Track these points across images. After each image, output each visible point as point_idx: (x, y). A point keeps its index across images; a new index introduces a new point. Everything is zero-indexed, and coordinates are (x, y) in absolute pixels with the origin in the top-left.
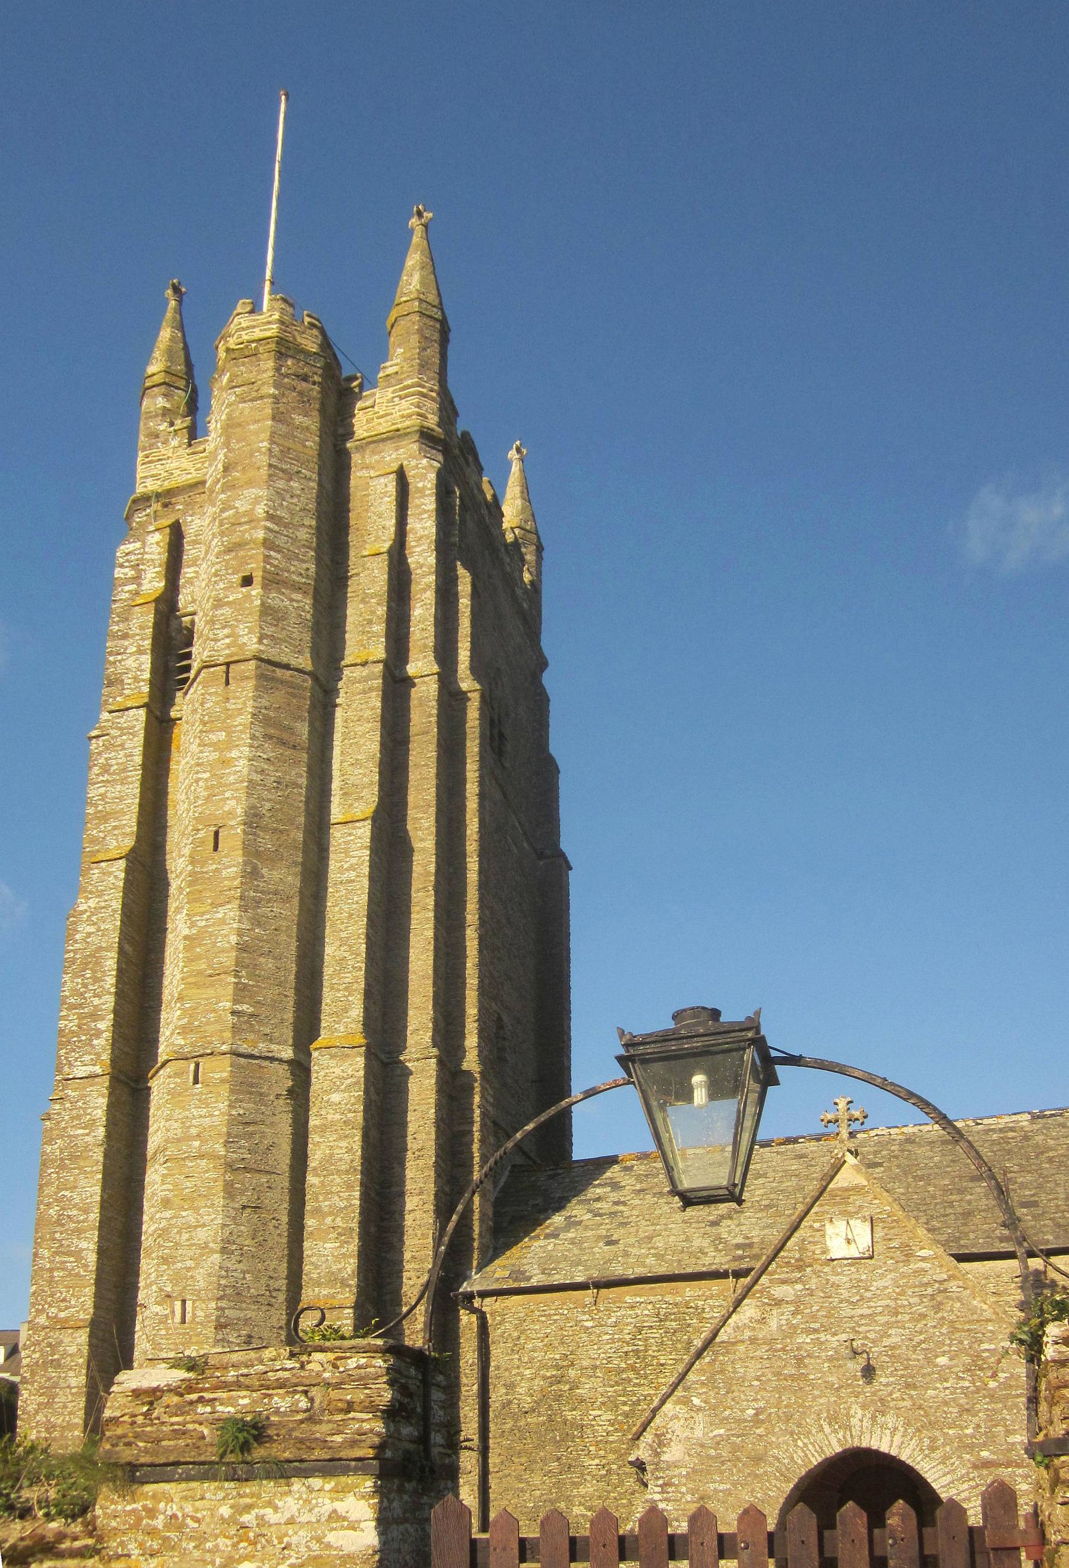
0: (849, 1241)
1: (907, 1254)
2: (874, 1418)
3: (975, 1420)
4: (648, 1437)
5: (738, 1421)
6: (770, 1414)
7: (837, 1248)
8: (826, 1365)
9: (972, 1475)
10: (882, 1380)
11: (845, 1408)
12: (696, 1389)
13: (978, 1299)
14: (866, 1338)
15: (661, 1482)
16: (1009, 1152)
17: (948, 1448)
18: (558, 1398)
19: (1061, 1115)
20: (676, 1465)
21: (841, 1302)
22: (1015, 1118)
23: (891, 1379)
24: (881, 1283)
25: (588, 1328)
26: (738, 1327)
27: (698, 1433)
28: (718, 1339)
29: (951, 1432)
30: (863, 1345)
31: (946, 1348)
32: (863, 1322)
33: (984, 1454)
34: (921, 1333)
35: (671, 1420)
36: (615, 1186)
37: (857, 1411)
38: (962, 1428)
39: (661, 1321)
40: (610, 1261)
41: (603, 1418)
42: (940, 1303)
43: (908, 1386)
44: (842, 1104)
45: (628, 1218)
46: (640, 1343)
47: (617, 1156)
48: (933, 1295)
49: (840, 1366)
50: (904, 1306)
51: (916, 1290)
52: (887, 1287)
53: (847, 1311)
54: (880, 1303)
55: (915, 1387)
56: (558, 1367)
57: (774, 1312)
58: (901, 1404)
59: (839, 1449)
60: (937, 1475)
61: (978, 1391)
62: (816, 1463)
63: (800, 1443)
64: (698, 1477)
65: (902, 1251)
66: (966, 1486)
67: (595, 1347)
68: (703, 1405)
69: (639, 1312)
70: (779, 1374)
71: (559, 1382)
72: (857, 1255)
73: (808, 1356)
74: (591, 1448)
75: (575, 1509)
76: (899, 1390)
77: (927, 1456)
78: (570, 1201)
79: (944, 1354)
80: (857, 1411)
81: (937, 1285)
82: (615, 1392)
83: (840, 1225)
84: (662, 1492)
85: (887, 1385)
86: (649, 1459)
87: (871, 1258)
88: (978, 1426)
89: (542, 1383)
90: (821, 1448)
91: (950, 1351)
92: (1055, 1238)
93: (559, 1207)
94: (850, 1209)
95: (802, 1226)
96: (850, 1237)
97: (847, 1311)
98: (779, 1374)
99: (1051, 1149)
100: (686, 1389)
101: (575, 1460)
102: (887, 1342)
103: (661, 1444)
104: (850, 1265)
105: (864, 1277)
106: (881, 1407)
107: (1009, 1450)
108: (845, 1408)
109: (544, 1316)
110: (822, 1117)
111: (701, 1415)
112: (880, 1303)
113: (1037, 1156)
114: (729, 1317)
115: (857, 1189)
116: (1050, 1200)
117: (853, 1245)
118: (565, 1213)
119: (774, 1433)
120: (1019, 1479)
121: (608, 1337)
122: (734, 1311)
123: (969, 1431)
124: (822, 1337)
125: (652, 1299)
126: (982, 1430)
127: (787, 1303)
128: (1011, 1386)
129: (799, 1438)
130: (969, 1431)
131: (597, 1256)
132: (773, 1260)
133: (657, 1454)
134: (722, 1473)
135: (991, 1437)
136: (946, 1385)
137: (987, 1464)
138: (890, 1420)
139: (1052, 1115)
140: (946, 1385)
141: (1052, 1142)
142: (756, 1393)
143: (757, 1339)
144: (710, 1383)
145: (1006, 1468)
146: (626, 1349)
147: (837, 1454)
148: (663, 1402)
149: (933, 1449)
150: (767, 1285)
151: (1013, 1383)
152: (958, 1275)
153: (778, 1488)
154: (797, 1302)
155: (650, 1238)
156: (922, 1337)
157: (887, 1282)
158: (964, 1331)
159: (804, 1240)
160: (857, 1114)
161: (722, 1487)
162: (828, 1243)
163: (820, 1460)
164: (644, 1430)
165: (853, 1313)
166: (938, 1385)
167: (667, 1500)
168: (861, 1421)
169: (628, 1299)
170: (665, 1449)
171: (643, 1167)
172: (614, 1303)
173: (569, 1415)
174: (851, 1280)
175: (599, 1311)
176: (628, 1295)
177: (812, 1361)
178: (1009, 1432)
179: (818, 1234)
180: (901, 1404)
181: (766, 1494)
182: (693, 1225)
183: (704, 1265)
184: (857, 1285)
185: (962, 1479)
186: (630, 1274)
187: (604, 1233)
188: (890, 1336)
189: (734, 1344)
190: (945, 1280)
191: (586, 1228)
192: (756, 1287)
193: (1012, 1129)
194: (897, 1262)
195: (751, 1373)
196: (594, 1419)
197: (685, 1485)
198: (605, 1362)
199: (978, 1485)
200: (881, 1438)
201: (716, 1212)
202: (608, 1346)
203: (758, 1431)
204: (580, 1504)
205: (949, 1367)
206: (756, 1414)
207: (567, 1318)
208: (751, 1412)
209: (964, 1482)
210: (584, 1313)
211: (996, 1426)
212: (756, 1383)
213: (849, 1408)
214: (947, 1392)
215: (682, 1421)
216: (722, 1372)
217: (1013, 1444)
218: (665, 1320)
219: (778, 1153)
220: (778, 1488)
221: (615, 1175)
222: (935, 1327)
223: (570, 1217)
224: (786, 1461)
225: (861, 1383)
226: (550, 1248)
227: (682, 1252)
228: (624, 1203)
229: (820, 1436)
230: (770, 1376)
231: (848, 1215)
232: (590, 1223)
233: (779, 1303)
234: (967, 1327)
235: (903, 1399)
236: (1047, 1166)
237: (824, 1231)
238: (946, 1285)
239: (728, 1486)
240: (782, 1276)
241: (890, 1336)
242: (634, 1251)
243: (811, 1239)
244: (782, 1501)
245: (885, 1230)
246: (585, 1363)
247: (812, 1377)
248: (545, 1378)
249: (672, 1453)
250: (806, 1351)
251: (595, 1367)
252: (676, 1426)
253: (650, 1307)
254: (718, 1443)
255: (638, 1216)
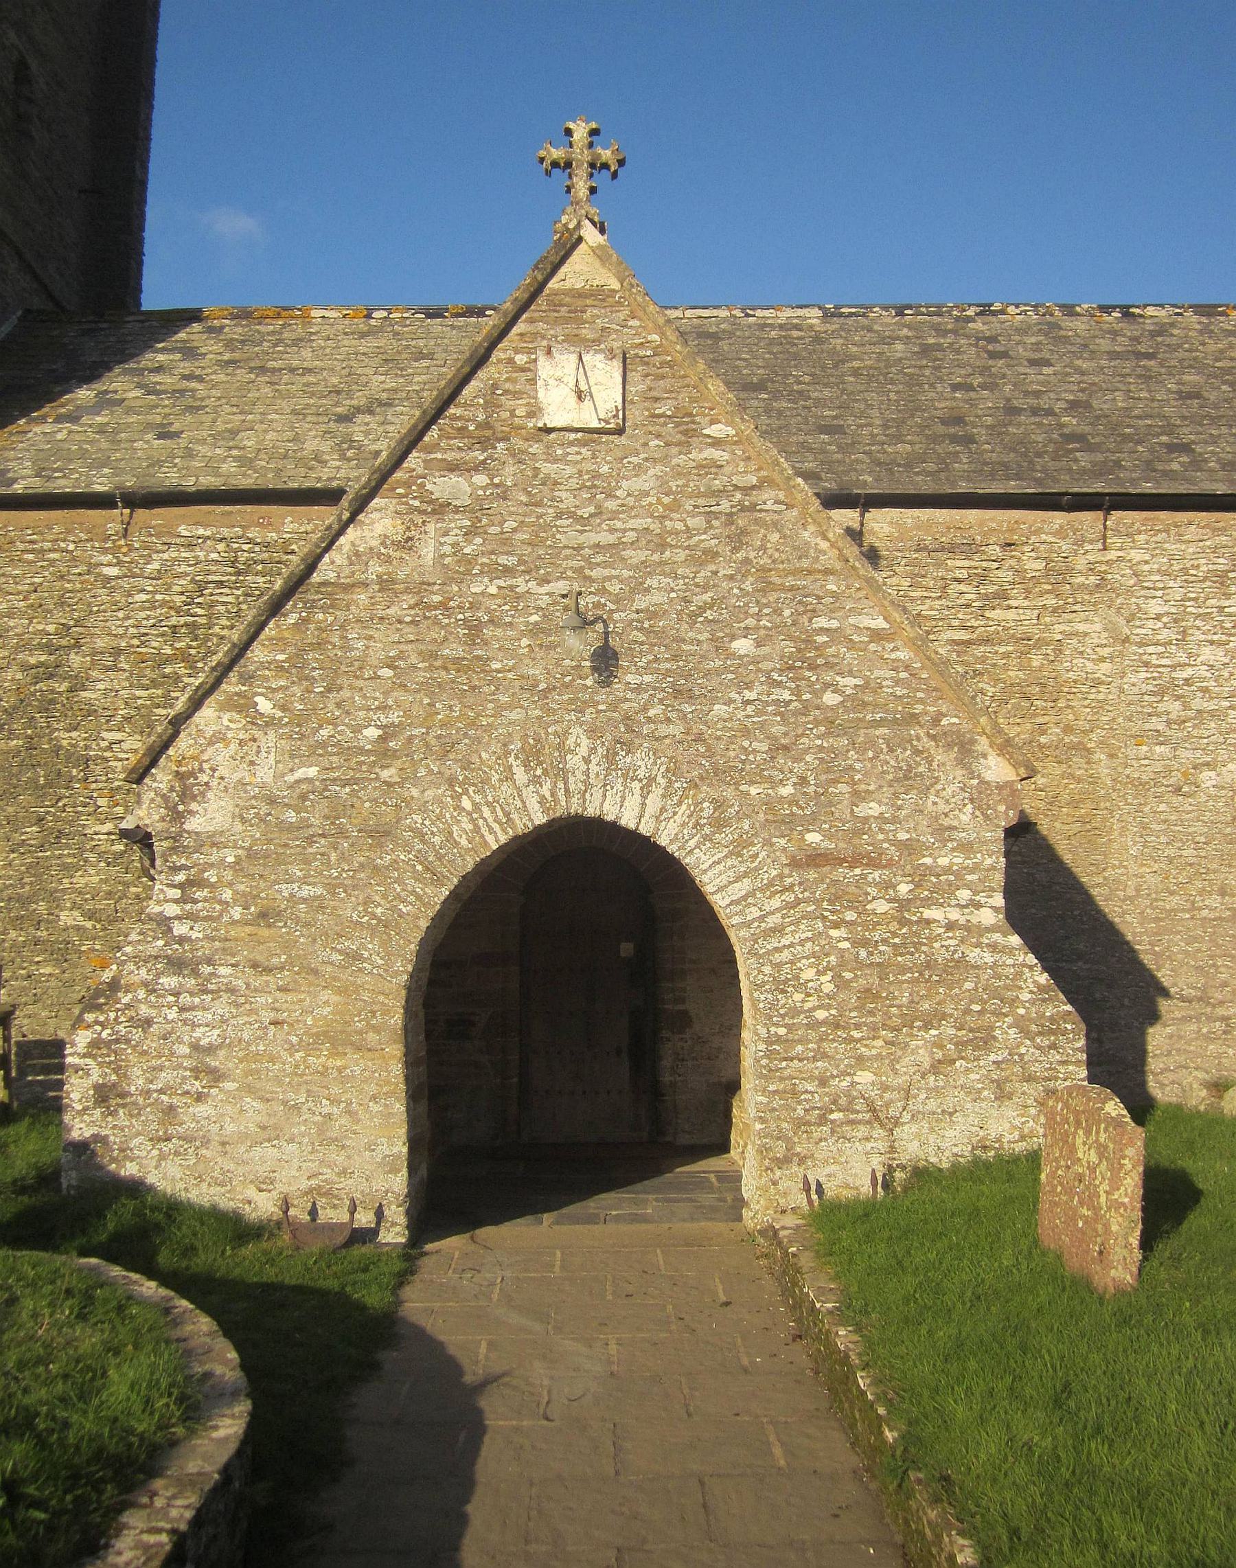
0: (580, 395)
1: (689, 434)
2: (610, 757)
3: (799, 768)
4: (161, 778)
5: (348, 752)
6: (410, 739)
7: (558, 407)
8: (525, 642)
9: (788, 881)
10: (630, 678)
11: (556, 734)
12: (267, 679)
13: (812, 528)
14: (603, 591)
15: (181, 877)
16: (795, 356)
17: (746, 824)
18: (47, 705)
19: (864, 315)
20: (214, 841)
21: (559, 516)
22: (800, 312)
23: (647, 679)
24: (636, 484)
25: (109, 579)
26: (357, 554)
27: (265, 773)
28: (316, 578)
29: (754, 791)
30: (597, 605)
31: (751, 622)
32: (600, 558)
33: (813, 838)
34: (705, 588)
35: (211, 743)
36: (189, 352)
37: (579, 740)
38: (774, 784)
39: (238, 573)
40: (159, 463)
41: (125, 746)
42: (744, 532)
43: (678, 693)
44: (580, 131)
45: (202, 399)
46: (199, 611)
47: (200, 310)
48: (731, 514)
49: (552, 646)
50: (677, 533)
51: (701, 502)
52: (647, 494)
53: (569, 535)
54: (632, 523)
55: (690, 696)
56: (49, 648)
57: (431, 527)
58: (663, 730)
59: (540, 819)
60: (724, 879)
61: (805, 711)
62: (495, 847)
63: (466, 803)
64: (257, 870)
65: (677, 425)
66: (776, 902)
67: (121, 614)
68: (279, 714)
69: (201, 555)
70: (433, 655)
71: (51, 676)
72: (595, 424)
73: (491, 621)
74: (100, 802)
75: (64, 915)
76: (661, 701)
77: (707, 838)
78: (110, 369)
79: (746, 632)
80: (579, 740)
81: (738, 496)
82: (150, 698)
83: (566, 362)
84: (182, 901)
85: (638, 689)
86: (160, 826)
87: (620, 431)
88: (803, 781)
89: (19, 676)
90: (507, 814)
91: (757, 628)
92: (876, 480)
93: (91, 374)
94: (586, 332)
95: (493, 359)
96: (583, 387)
97: (569, 535)
98: (433, 655)
99: (854, 358)
100: (246, 679)
101: (70, 823)
102: (641, 602)
103: (186, 795)
104: (584, 443)
105: (605, 469)
106: (622, 737)
107: (858, 833)
108: (556, 734)
109: (32, 552)
110: (542, 153)
111: (272, 735)
112: (632, 523)
113: (836, 366)
114: (341, 532)
115: (599, 295)
116: (860, 426)
117: (588, 403)
118: (99, 386)
119: (416, 781)
120: (873, 891)
121: (144, 597)
122: (352, 520)
123: (786, 791)
124: (521, 584)
125: (226, 532)
126: (811, 789)
127: (457, 510)
128: (865, 704)
129: (466, 792)
130: (786, 791)
131: (140, 453)
132: (433, 420)
133: (177, 817)
134: (307, 862)
135: (825, 801)
136: (749, 695)
137: (816, 859)
138: (641, 761)
139: (851, 315)
140: (749, 695)
141: (855, 349)
142: (386, 694)
143: (394, 582)
144: (296, 667)
145: (851, 867)
146: (174, 621)
147: (538, 829)
148: (196, 703)
149: (719, 824)
150: (420, 471)
151: (869, 698)
152: (778, 479)
153: (419, 898)
154: (477, 509)
155: (234, 433)
156: (707, 597)
157: (646, 482)
158: (782, 588)
159: (495, 386)
160: (606, 155)
161: (308, 891)
162: (541, 394)
163: (503, 839)
164: (154, 763)
165: (582, 539)
166: (734, 695)
167: (192, 917)
168: (587, 761)
169: (183, 530)
170: (194, 806)
171: (240, 330)
172: (158, 536)
173: (65, 738)
174: (580, 472)
175: (131, 549)
176: (186, 524)
177: (499, 632)
178: (859, 796)
179: (523, 377)
180: (663, 730)
181: (393, 909)
182: (309, 419)
183: (319, 479)
184: (593, 485)
185: (770, 888)
186: (190, 484)
187: (158, 420)
188: (648, 590)
189: (347, 588)
190: (753, 487)
191: (129, 411)
192: (398, 475)
193: (797, 327)
194: (667, 445)
195: (378, 652)
196: (109, 748)
197: (230, 885)
198: (135, 642)
199: (798, 902)
200: (623, 799)
201: (348, 402)
202: (143, 614)
203: (385, 774)
204: (75, 907)
205: (756, 661)
206: (383, 739)
207: (74, 559)
208: (372, 733)
209: (774, 894)
210: (105, 551)
211: (835, 782)
212: (386, 672)
213: (566, 733)
214: (750, 709)
215: (234, 746)
216: (320, 645)
217: (866, 819)
218: (247, 573)
219: (453, 327)
220: (419, 898)
221: (192, 337)
222: (731, 578)
223: (106, 392)
224: (437, 840)
225: (589, 682)
226: (59, 436)
227: (285, 457)
228: (200, 379)
229: (507, 790)
230: (414, 659)
231: (580, 344)
232: (139, 403)
233: (440, 509)
234: (790, 581)
235: (668, 720)
236: (852, 379)
237: (535, 372)
238: (755, 496)
239: (319, 891)
240: (449, 456)
241: (648, 590)
242: (203, 450)
243: (507, 386)
244: (424, 924)
245: (649, 380)
246: (100, 644)
247: (496, 665)
248: (25, 667)
249: (208, 816)
250: (488, 611)
251: (117, 652)
252: (221, 756)
253: (221, 546)
254: (303, 797)
255: (219, 398)
